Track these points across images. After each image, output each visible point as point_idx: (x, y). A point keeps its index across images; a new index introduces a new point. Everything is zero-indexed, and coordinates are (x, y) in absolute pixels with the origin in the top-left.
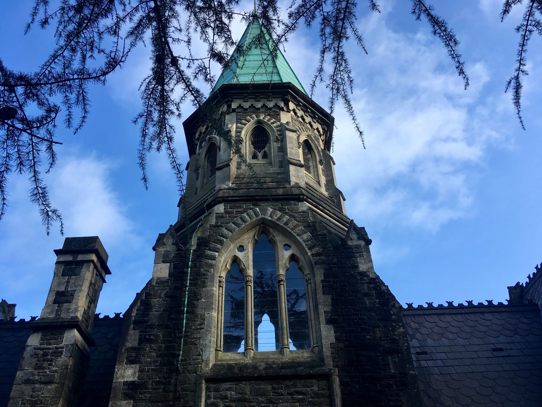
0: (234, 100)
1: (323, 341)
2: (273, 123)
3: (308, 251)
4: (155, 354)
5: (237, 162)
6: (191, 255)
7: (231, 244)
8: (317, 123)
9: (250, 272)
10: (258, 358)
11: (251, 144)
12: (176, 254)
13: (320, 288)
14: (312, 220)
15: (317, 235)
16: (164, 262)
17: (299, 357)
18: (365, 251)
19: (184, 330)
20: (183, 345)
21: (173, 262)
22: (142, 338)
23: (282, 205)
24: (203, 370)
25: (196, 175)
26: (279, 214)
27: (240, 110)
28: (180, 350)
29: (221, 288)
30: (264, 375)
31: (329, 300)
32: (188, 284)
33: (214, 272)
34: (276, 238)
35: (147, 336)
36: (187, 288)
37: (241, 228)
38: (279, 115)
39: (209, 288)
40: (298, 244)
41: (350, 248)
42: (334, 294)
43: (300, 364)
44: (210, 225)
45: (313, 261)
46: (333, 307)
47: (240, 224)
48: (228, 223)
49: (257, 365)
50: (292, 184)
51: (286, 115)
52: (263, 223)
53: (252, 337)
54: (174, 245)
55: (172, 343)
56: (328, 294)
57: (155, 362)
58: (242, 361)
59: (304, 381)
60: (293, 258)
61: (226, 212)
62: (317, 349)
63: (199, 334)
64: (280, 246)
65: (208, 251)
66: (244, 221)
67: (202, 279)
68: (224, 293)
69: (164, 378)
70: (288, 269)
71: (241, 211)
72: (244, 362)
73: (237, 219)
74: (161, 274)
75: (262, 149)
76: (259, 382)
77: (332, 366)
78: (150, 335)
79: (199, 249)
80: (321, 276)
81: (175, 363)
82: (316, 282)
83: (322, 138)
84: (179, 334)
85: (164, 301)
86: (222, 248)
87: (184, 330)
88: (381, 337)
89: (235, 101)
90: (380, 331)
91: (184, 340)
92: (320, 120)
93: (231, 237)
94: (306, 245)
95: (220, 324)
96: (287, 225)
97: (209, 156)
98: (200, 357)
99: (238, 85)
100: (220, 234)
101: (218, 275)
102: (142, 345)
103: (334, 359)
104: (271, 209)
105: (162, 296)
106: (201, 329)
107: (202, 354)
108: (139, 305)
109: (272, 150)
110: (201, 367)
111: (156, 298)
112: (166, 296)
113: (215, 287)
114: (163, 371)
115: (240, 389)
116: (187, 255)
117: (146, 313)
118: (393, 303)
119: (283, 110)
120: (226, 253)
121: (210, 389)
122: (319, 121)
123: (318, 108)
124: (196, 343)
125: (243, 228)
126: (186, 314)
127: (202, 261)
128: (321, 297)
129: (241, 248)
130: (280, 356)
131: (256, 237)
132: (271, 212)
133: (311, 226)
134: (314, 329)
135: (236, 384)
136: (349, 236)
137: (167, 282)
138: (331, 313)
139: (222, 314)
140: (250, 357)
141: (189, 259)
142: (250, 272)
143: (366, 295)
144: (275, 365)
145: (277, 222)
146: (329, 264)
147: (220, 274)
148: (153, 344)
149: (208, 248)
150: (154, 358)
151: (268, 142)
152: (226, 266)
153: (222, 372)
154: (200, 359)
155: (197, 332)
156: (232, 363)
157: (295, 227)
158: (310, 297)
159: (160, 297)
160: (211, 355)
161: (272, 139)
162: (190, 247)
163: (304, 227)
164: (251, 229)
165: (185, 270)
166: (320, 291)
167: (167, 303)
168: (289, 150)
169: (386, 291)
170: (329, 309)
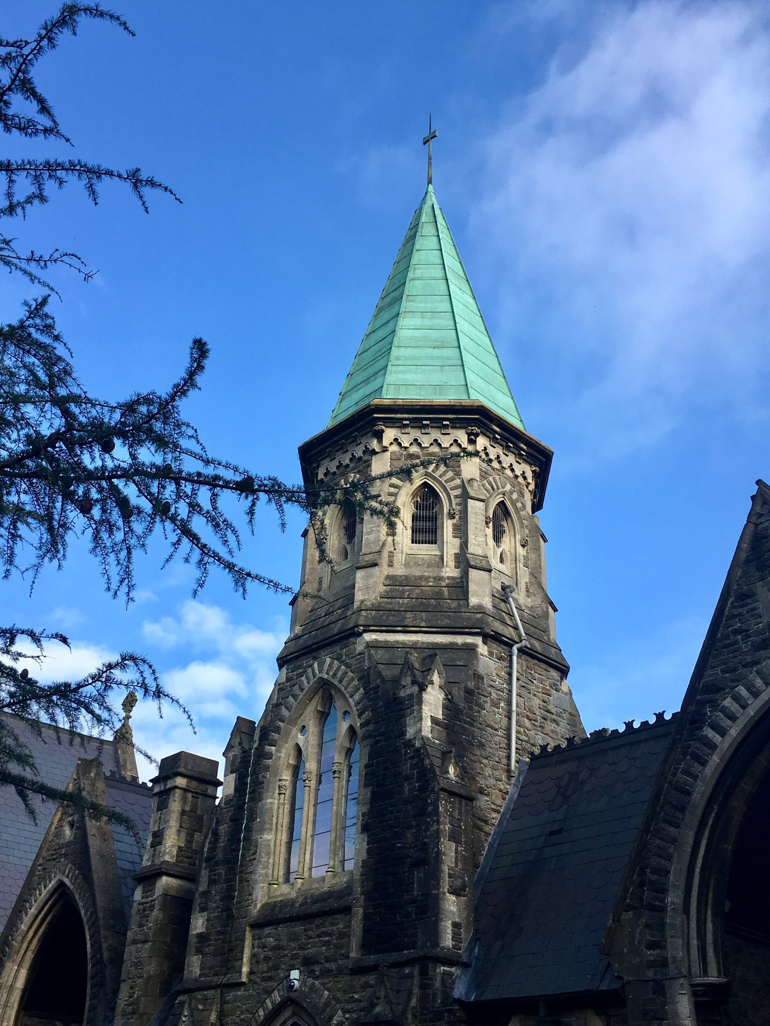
0: (322, 462)
57: (218, 907)
59: (330, 918)
164: (313, 697)
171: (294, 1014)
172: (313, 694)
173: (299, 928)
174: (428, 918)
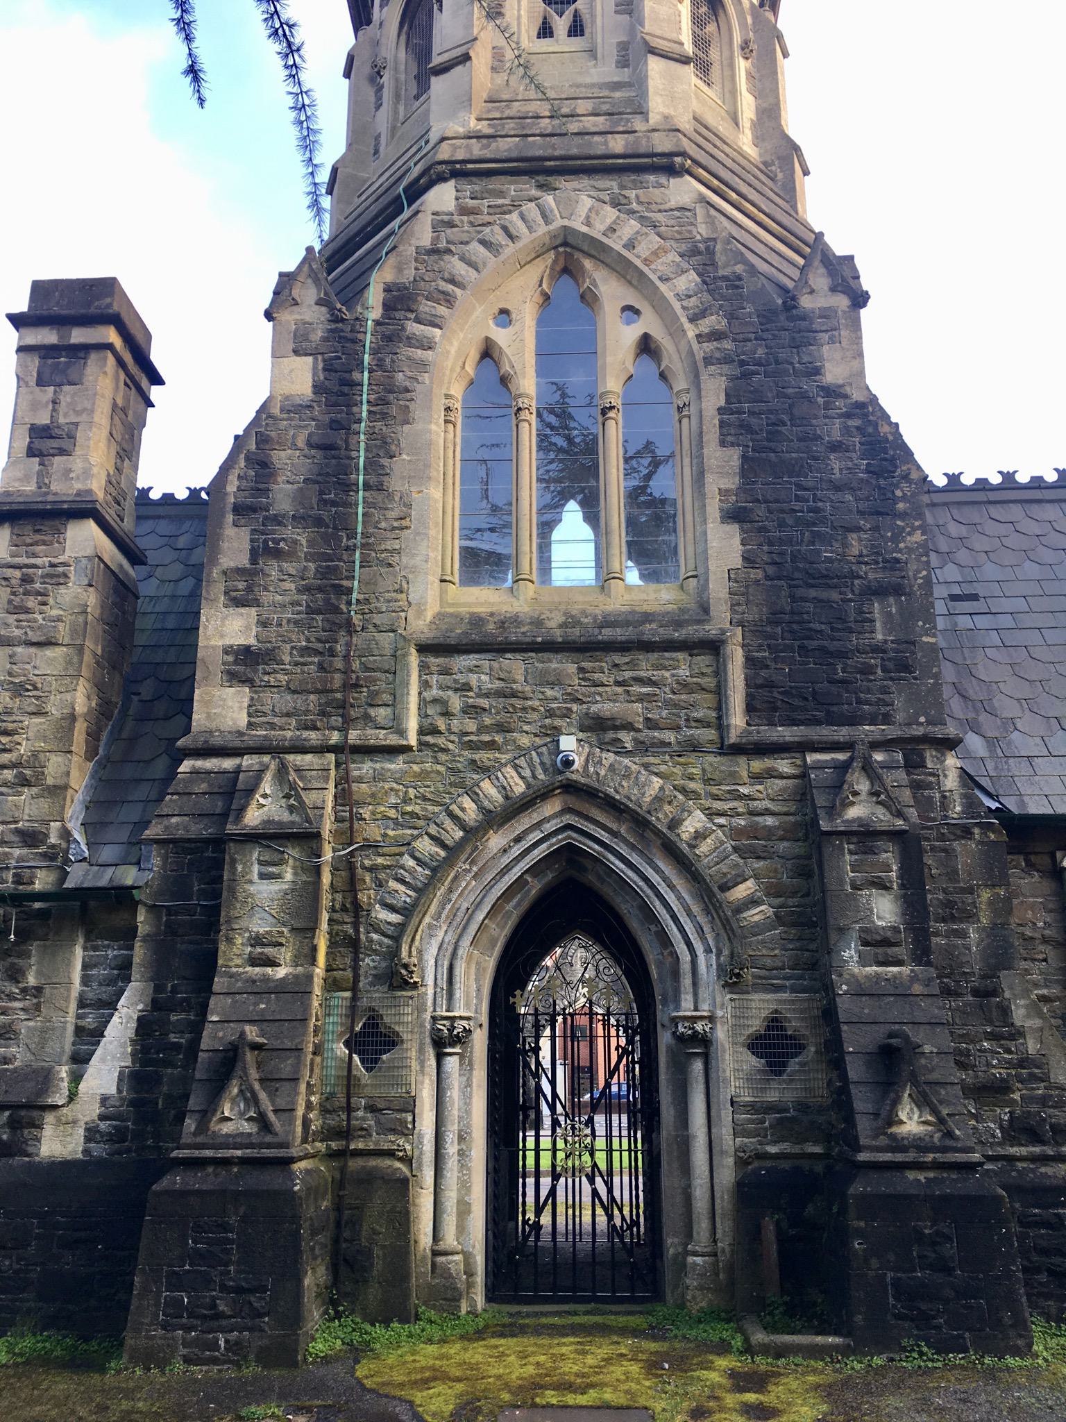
164: (530, 262)
171: (567, 810)
172: (534, 255)
173: (568, 667)
174: (915, 678)
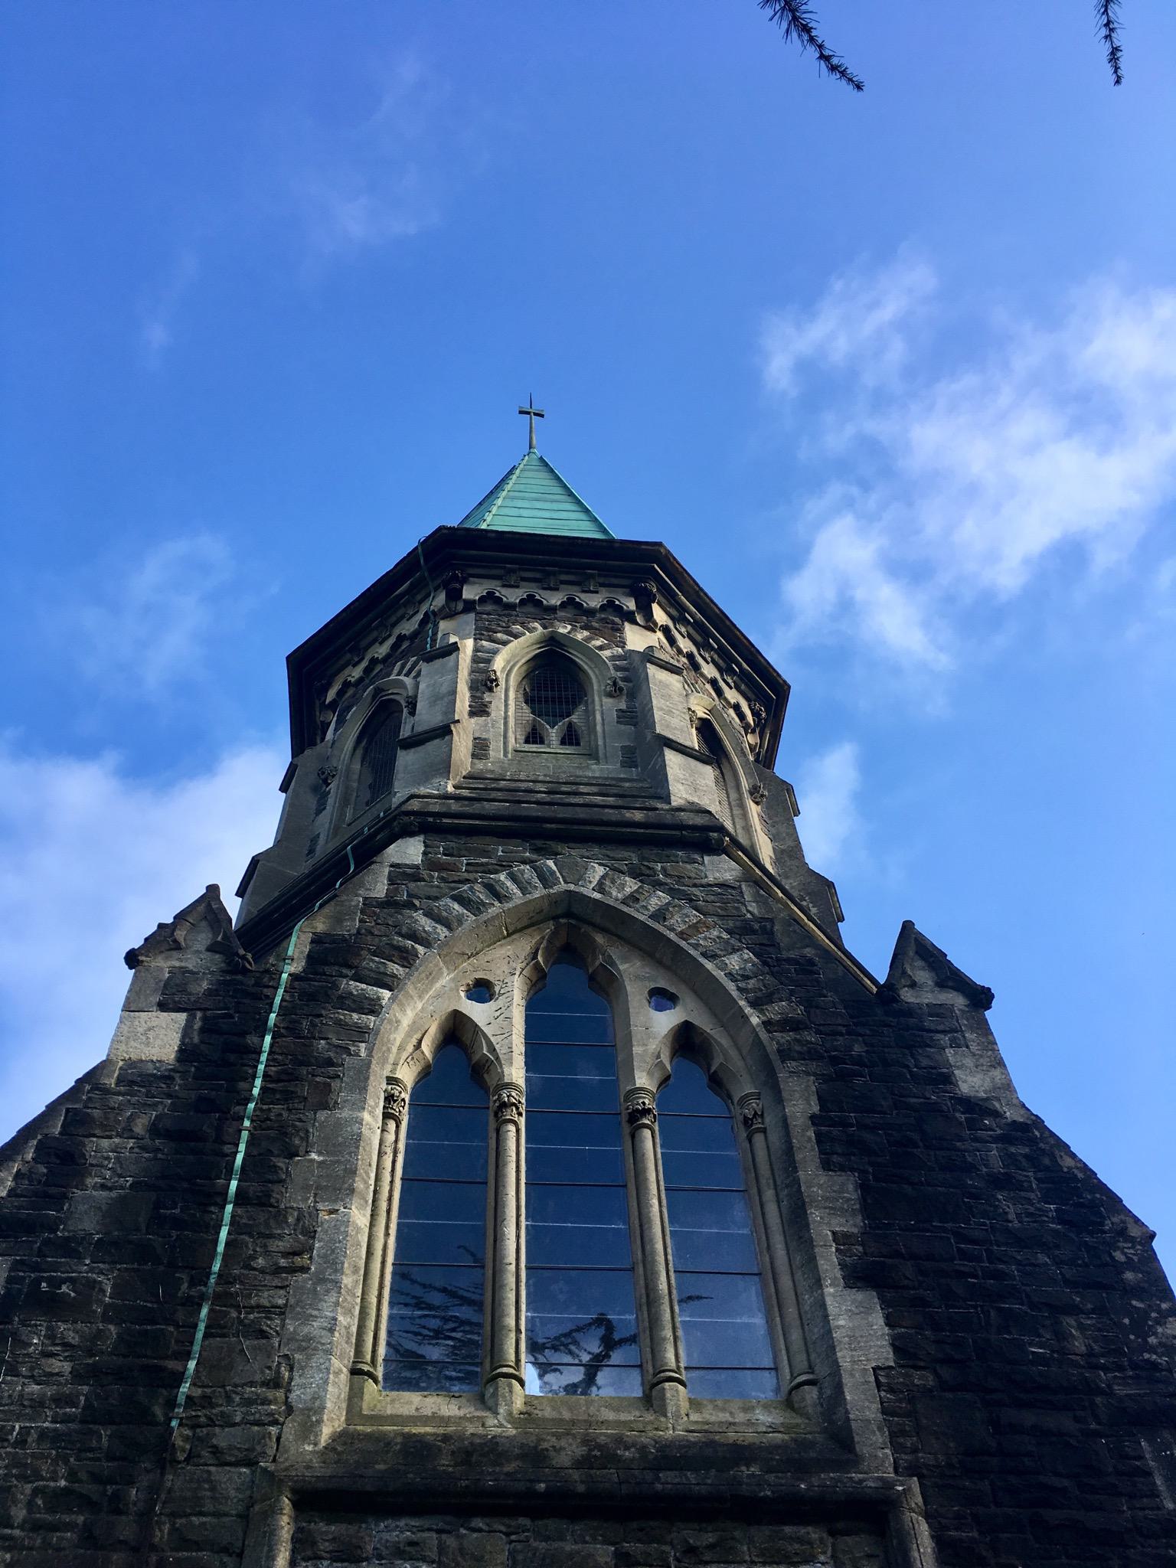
1: (839, 1354)
2: (601, 648)
3: (748, 1010)
4: (67, 1367)
5: (475, 739)
6: (281, 991)
7: (445, 969)
8: (734, 690)
9: (516, 1072)
10: (544, 1420)
11: (522, 699)
12: (224, 983)
13: (809, 1146)
14: (756, 912)
15: (778, 960)
16: (163, 1007)
17: (734, 1424)
18: (972, 1030)
19: (216, 1267)
20: (206, 1336)
21: (204, 1010)
22: (20, 1290)
23: (642, 858)
24: (287, 1451)
25: (318, 801)
26: (631, 885)
27: (489, 608)
28: (188, 1356)
29: (392, 1125)
30: (581, 1488)
31: (851, 1193)
32: (256, 1091)
33: (370, 1054)
34: (621, 967)
35: (44, 1284)
36: (251, 1106)
37: (484, 917)
38: (620, 630)
39: (345, 1113)
40: (707, 991)
41: (909, 1011)
42: (867, 1172)
43: (741, 1453)
44: (365, 899)
45: (772, 1047)
46: (868, 1218)
47: (484, 904)
48: (437, 899)
49: (545, 1445)
50: (676, 802)
51: (641, 635)
52: (568, 914)
53: (518, 1331)
54: (216, 952)
55: (154, 1322)
56: (842, 1168)
57: (59, 1400)
58: (471, 1429)
59: (766, 1530)
60: (686, 1041)
61: (430, 863)
62: (811, 1394)
63: (282, 1292)
64: (635, 994)
65: (352, 982)
66: (499, 896)
67: (318, 1079)
68: (401, 1146)
69: (95, 1478)
70: (668, 1078)
71: (487, 864)
72: (480, 1430)
73: (471, 889)
74: (146, 1050)
75: (562, 717)
76: (551, 1524)
77: (891, 1470)
78: (56, 1283)
79: (316, 973)
80: (807, 1100)
81: (158, 1411)
82: (792, 1123)
83: (752, 739)
84: (189, 1287)
85: (143, 1148)
86: (408, 976)
87: (216, 1267)
88: (1091, 1354)
89: (474, 583)
90: (1081, 1327)
91: (211, 1311)
92: (746, 684)
93: (446, 943)
94: (739, 989)
95: (378, 1265)
96: (665, 919)
97: (369, 743)
98: (280, 1394)
99: (489, 535)
100: (404, 930)
101: (386, 1073)
102: (11, 1322)
103: (895, 1438)
104: (602, 868)
105: (140, 1126)
106: (294, 1270)
107: (291, 1379)
108: (29, 1156)
109: (598, 717)
110: (278, 1439)
111: (110, 1137)
112: (154, 1130)
113: (370, 1112)
114: (94, 1444)
115: (461, 1550)
116: (265, 990)
117: (53, 1190)
118: (1115, 1220)
119: (634, 622)
120: (420, 997)
121: (314, 1543)
122: (743, 687)
123: (742, 642)
124: (264, 1328)
125: (493, 918)
126: (236, 1204)
127: (324, 1012)
128: (814, 1179)
129: (482, 990)
130: (649, 1417)
131: (540, 958)
132: (603, 877)
133: (754, 932)
134: (791, 1311)
135: (441, 1525)
136: (904, 972)
137: (167, 1078)
138: (862, 1244)
139: (387, 1227)
140: (510, 1414)
141: (271, 1004)
142: (516, 1072)
143: (1000, 1182)
144: (627, 1448)
145: (625, 909)
146: (834, 1061)
147: (393, 1071)
148: (65, 1321)
149: (351, 973)
150: (59, 1384)
151: (581, 699)
152: (418, 1046)
153: (381, 1467)
154: (274, 1401)
155: (276, 1282)
156: (428, 1434)
157: (695, 928)
158: (763, 1181)
159: (128, 1132)
160: (330, 1388)
161: (595, 687)
162: (281, 964)
163: (729, 932)
165: (251, 1040)
166: (808, 1156)
167: (155, 1159)
168: (657, 715)
169: (1080, 1175)
170: (855, 1226)
